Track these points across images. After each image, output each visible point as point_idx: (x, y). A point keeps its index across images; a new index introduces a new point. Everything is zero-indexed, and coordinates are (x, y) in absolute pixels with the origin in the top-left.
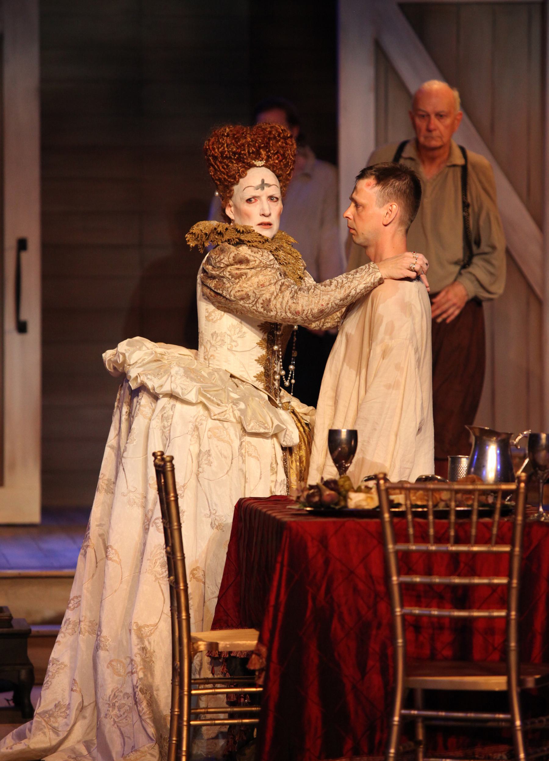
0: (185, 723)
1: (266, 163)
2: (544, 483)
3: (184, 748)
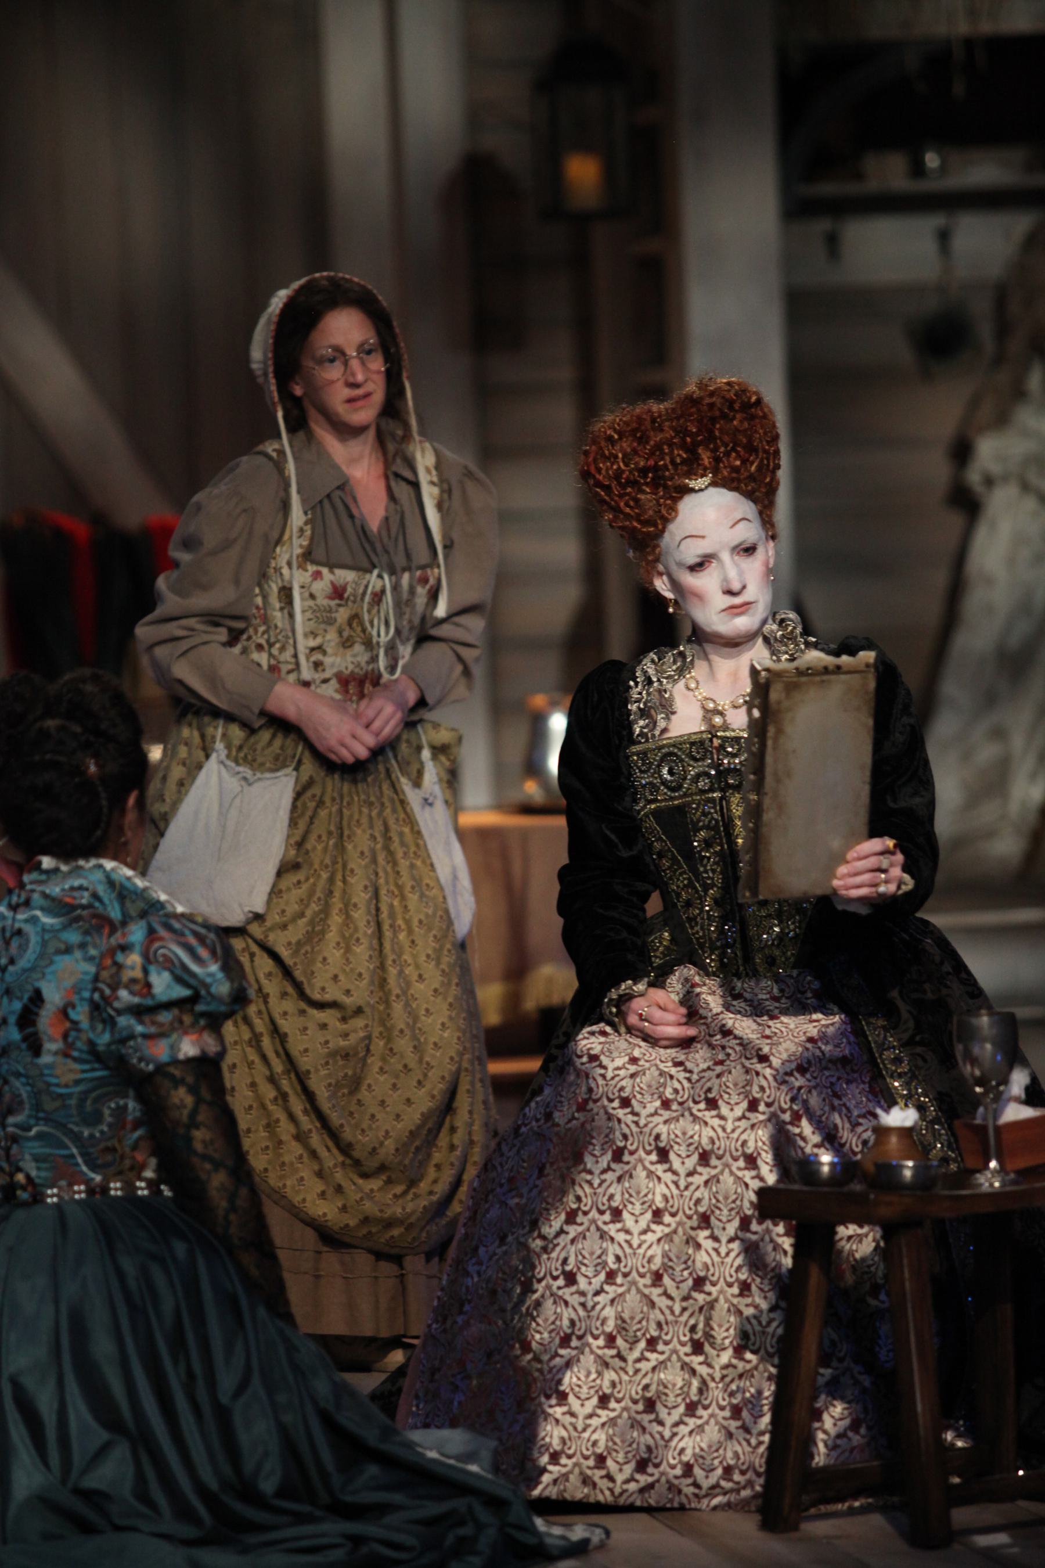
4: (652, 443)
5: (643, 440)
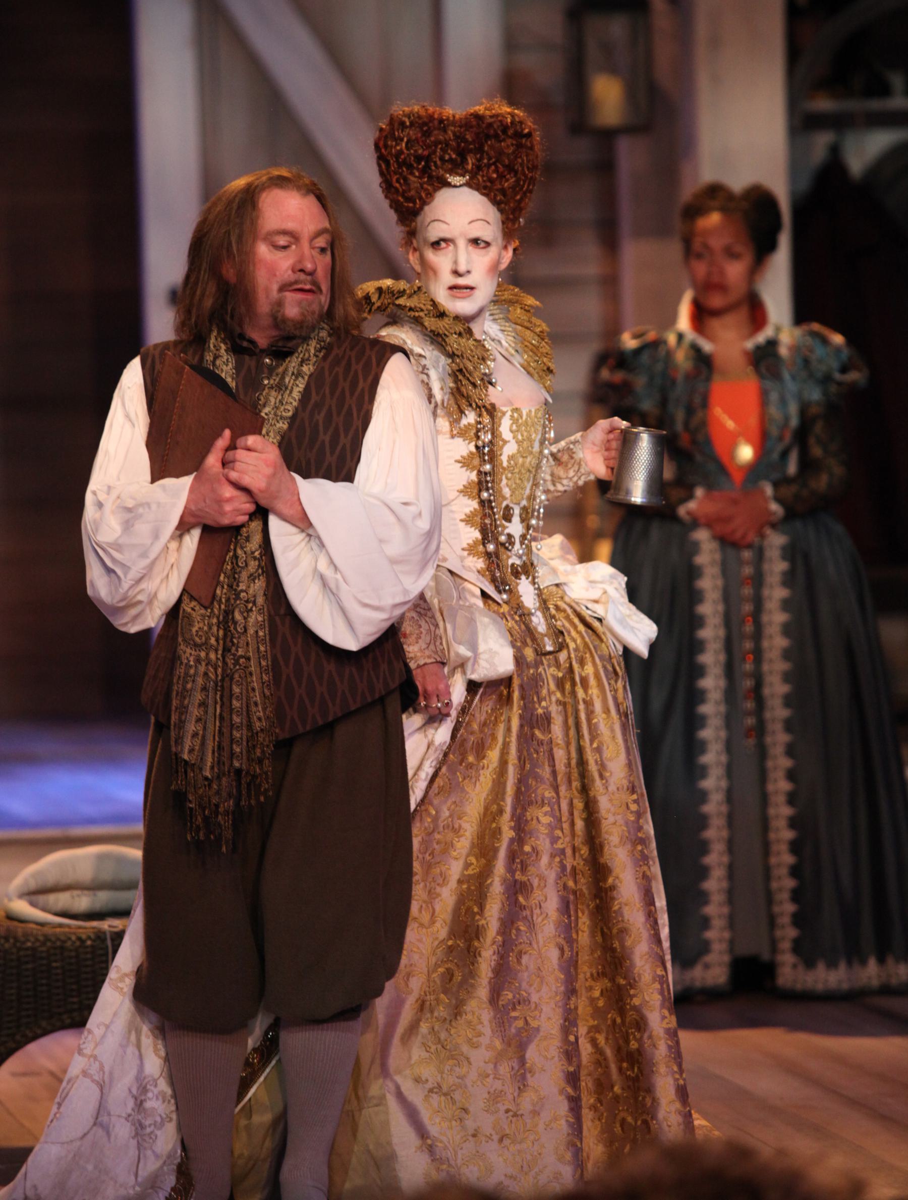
2: (447, 969)
4: (432, 139)
5: (427, 134)
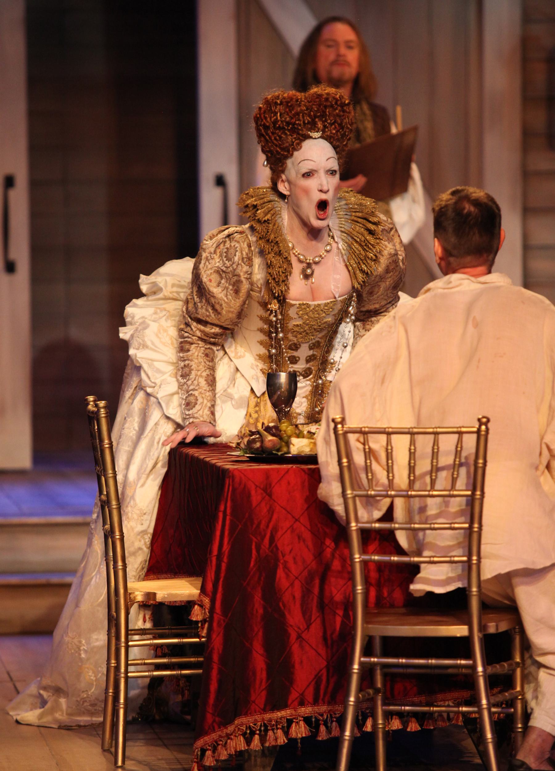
0: (123, 675)
1: (322, 134)
3: (122, 701)
